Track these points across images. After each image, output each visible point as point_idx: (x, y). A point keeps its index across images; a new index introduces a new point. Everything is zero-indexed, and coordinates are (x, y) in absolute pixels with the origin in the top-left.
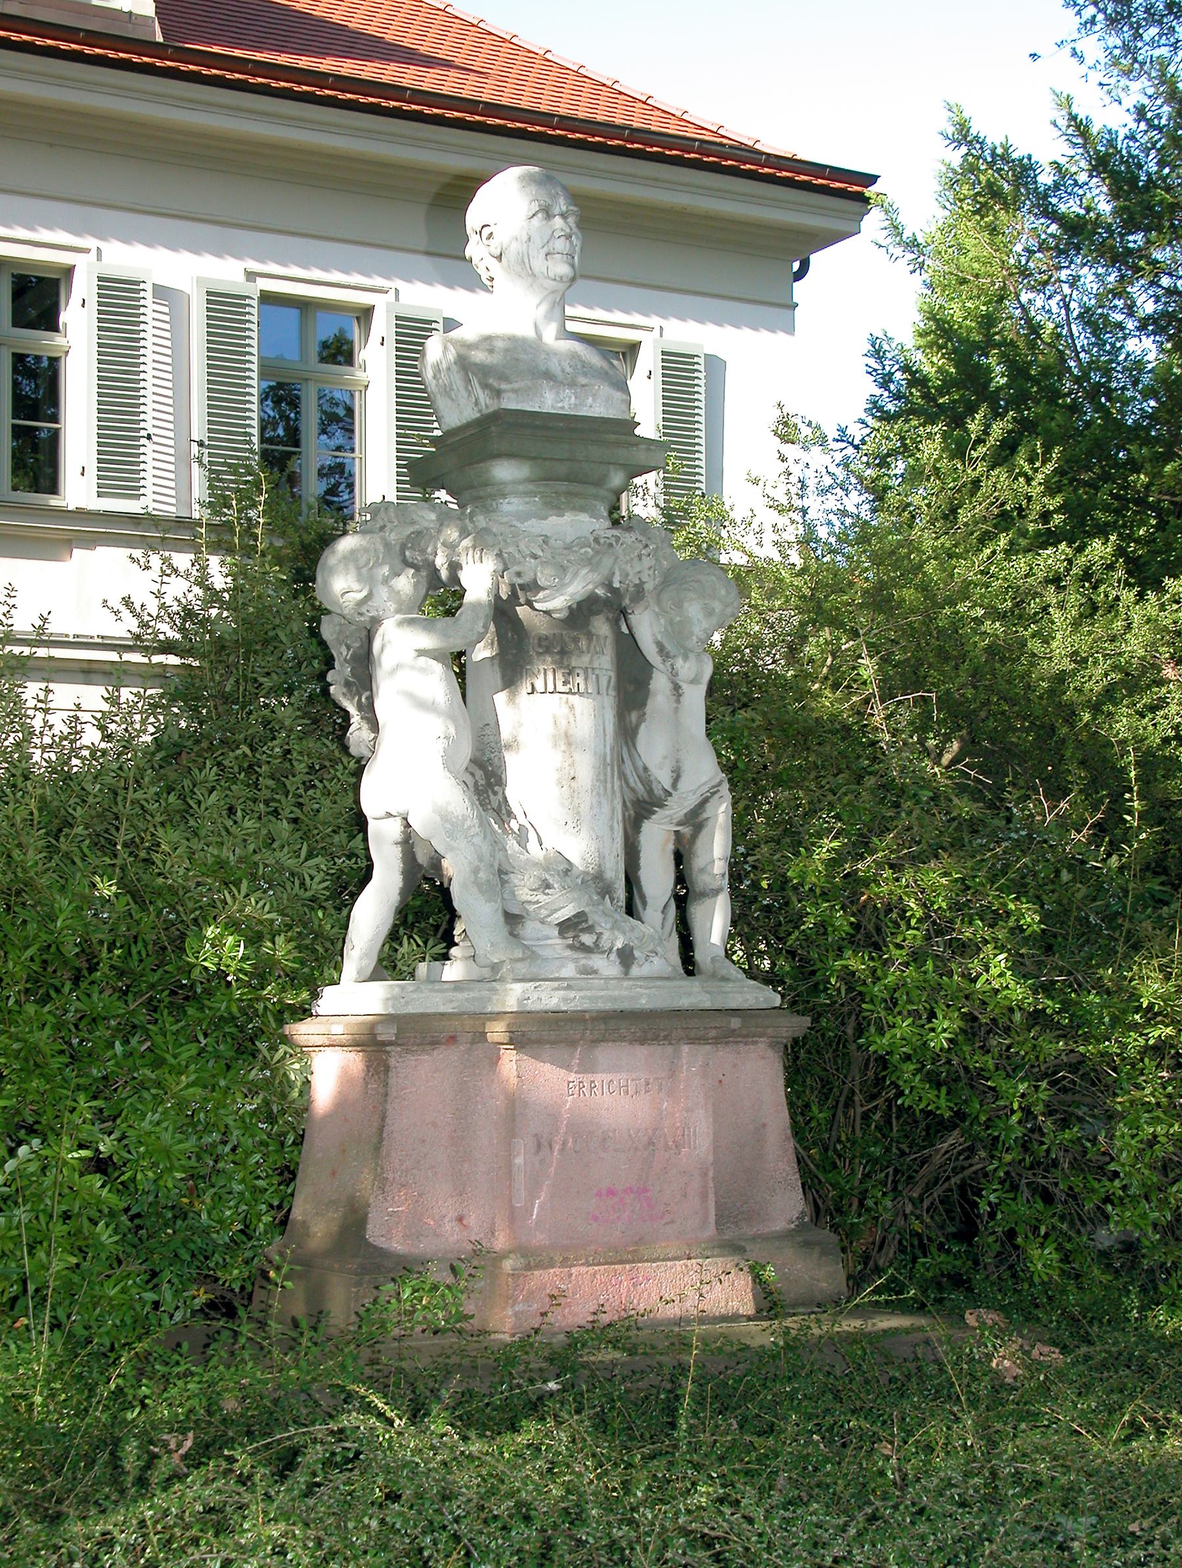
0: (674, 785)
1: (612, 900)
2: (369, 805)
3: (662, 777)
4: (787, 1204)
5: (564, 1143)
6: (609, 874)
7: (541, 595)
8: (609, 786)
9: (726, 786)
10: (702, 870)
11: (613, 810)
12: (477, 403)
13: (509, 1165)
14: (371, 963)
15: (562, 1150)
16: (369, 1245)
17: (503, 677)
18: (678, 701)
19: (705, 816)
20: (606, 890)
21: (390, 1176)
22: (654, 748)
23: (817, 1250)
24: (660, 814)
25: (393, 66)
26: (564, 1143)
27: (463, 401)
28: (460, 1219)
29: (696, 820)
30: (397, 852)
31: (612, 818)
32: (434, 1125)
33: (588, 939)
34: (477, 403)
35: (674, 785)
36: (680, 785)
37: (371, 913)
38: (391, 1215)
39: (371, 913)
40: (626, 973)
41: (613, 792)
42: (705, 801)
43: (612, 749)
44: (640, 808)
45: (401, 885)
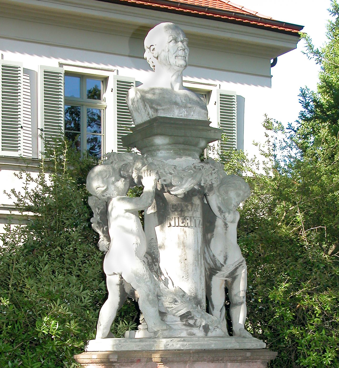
0: (225, 262)
3: (220, 259)
6: (200, 297)
8: (200, 262)
9: (245, 262)
10: (236, 295)
11: (201, 272)
12: (148, 114)
14: (107, 331)
19: (237, 274)
20: (198, 303)
22: (217, 248)
24: (219, 273)
27: (143, 114)
31: (201, 275)
33: (191, 322)
34: (148, 114)
35: (225, 262)
37: (108, 312)
39: (108, 312)
40: (206, 335)
41: (201, 265)
42: (236, 269)
43: (201, 248)
44: (211, 271)
45: (119, 301)
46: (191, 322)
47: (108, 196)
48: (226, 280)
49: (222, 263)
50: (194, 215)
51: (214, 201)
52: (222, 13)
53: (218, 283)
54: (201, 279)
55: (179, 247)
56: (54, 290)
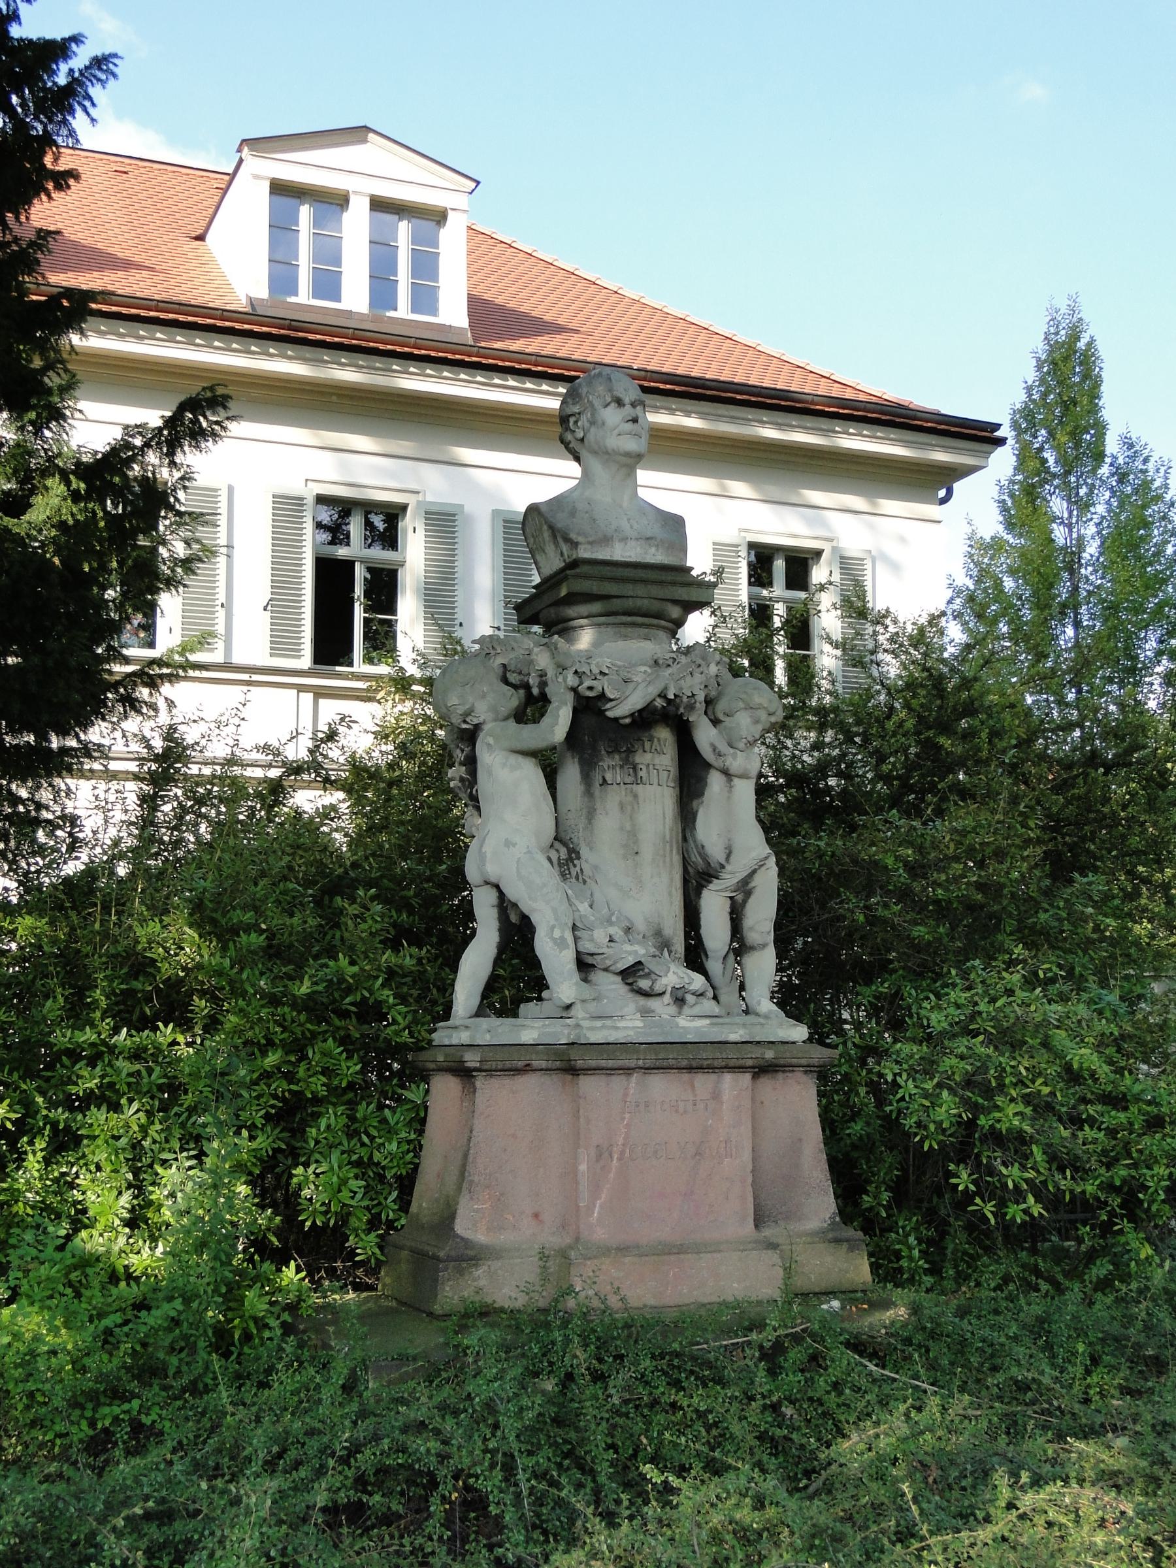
0: (728, 859)
1: (670, 952)
2: (472, 871)
3: (716, 852)
4: (821, 1205)
5: (622, 1153)
6: (668, 931)
7: (608, 706)
9: (773, 859)
10: (751, 929)
11: (672, 880)
12: (562, 554)
13: (575, 1171)
14: (476, 1001)
15: (619, 1159)
16: (458, 1236)
17: (582, 772)
18: (730, 792)
20: (664, 945)
21: (476, 1179)
22: (710, 831)
23: (845, 1246)
24: (715, 885)
25: (70, 274)
26: (622, 1153)
28: (536, 1216)
29: (745, 888)
30: (494, 913)
32: (514, 1136)
35: (728, 859)
36: (732, 859)
37: (476, 963)
38: (477, 1211)
39: (476, 963)
41: (672, 865)
42: (754, 872)
43: (671, 830)
44: (696, 878)
46: (644, 984)
47: (476, 721)
48: (731, 898)
49: (723, 862)
50: (657, 761)
51: (705, 736)
52: (806, 429)
53: (714, 908)
54: (670, 894)
55: (772, 998)
56: (511, 1374)
